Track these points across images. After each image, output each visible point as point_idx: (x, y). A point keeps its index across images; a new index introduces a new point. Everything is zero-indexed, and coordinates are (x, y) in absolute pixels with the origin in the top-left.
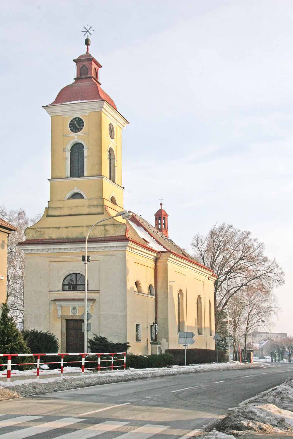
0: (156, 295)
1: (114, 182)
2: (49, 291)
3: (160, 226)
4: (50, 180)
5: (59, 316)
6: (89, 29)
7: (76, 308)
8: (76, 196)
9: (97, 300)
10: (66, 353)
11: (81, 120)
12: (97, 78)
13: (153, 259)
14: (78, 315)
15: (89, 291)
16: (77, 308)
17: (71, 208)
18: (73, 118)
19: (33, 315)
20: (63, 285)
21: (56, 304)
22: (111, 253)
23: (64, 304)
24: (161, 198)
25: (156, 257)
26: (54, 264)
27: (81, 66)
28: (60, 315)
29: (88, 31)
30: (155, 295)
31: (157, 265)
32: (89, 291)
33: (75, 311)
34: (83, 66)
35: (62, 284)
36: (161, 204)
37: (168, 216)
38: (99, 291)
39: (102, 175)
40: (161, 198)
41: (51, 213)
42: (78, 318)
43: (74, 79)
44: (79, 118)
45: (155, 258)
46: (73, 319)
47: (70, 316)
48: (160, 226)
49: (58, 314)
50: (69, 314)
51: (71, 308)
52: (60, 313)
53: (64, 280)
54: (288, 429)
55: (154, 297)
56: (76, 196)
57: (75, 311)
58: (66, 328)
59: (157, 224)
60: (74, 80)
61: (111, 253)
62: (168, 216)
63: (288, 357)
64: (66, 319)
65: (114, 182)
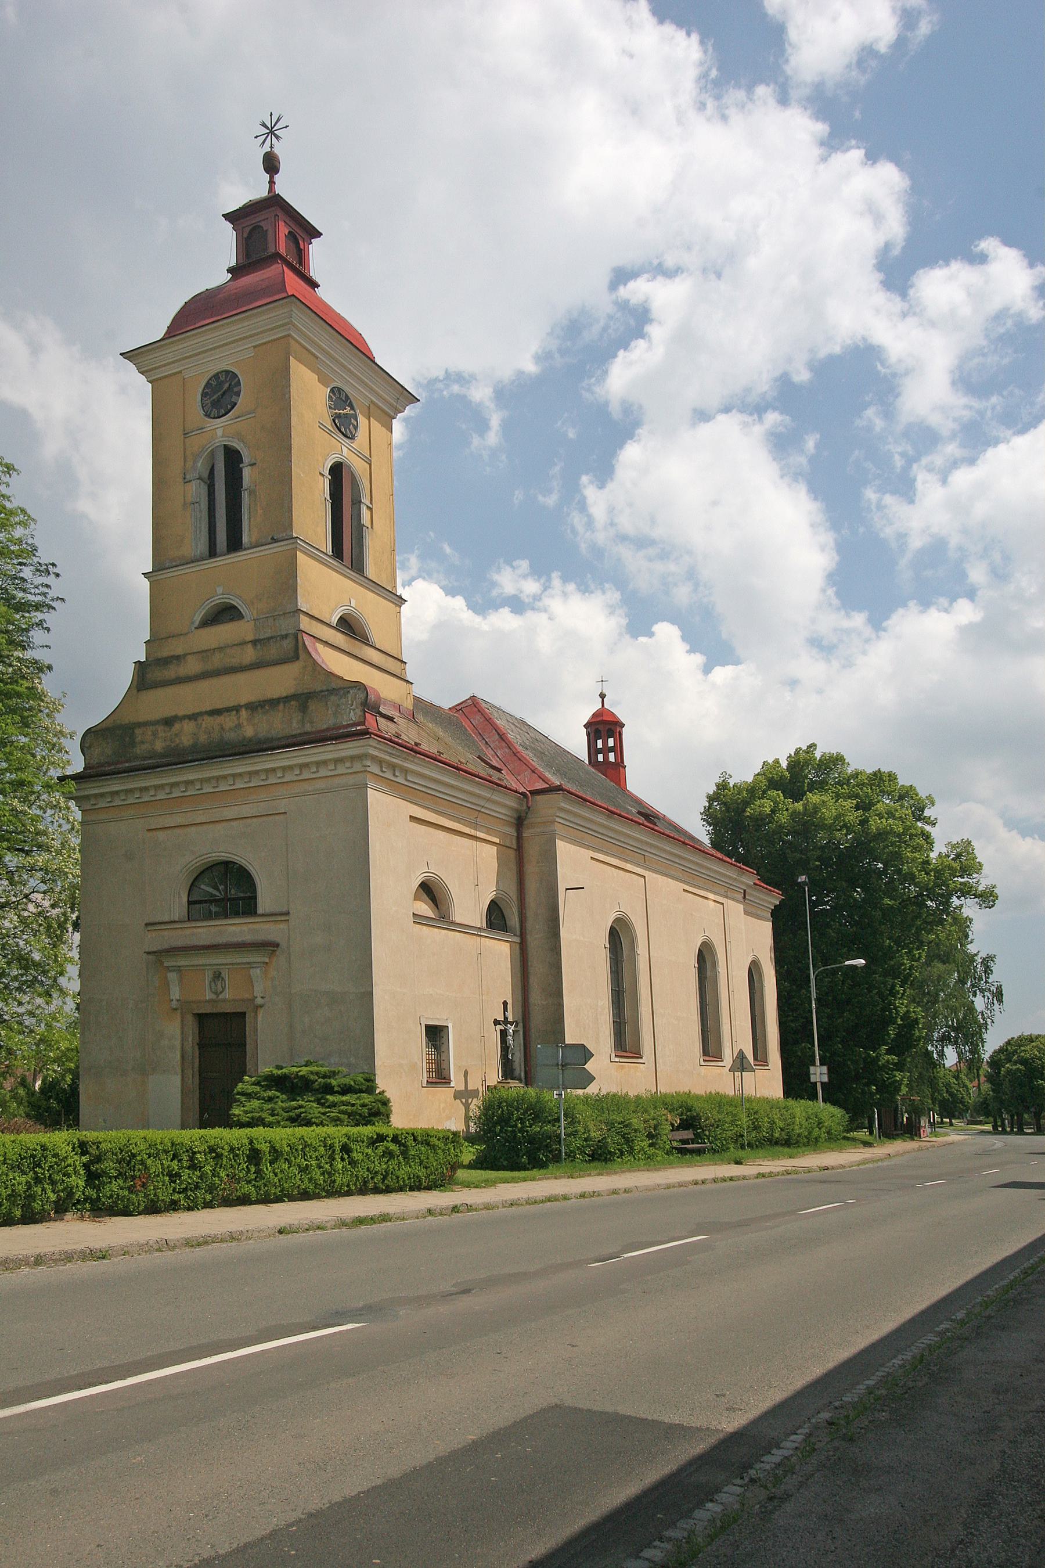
0: (523, 936)
1: (357, 566)
2: (147, 925)
3: (600, 757)
4: (151, 575)
5: (174, 1005)
6: (275, 125)
7: (223, 975)
8: (225, 613)
9: (283, 944)
10: (203, 1125)
11: (235, 375)
12: (301, 264)
13: (511, 817)
14: (230, 997)
15: (263, 915)
16: (225, 974)
17: (204, 654)
18: (212, 374)
19: (104, 1003)
20: (190, 903)
21: (162, 963)
22: (321, 785)
23: (186, 963)
24: (602, 677)
25: (517, 810)
26: (161, 835)
27: (248, 230)
28: (178, 1001)
29: (272, 132)
30: (518, 933)
31: (524, 835)
32: (263, 915)
33: (219, 986)
34: (254, 229)
35: (185, 900)
36: (602, 696)
37: (622, 725)
38: (288, 913)
39: (295, 535)
40: (602, 677)
41: (158, 674)
42: (228, 1009)
43: (229, 271)
44: (227, 372)
45: (515, 816)
46: (215, 1011)
47: (206, 1001)
48: (600, 757)
49: (171, 998)
50: (204, 995)
51: (209, 975)
52: (175, 993)
53: (192, 884)
54: (1041, 1325)
55: (517, 940)
56: (225, 613)
57: (219, 986)
58: (197, 1040)
59: (593, 751)
60: (230, 276)
61: (321, 785)
62: (622, 725)
63: (1034, 1121)
64: (196, 1011)
65: (357, 566)
